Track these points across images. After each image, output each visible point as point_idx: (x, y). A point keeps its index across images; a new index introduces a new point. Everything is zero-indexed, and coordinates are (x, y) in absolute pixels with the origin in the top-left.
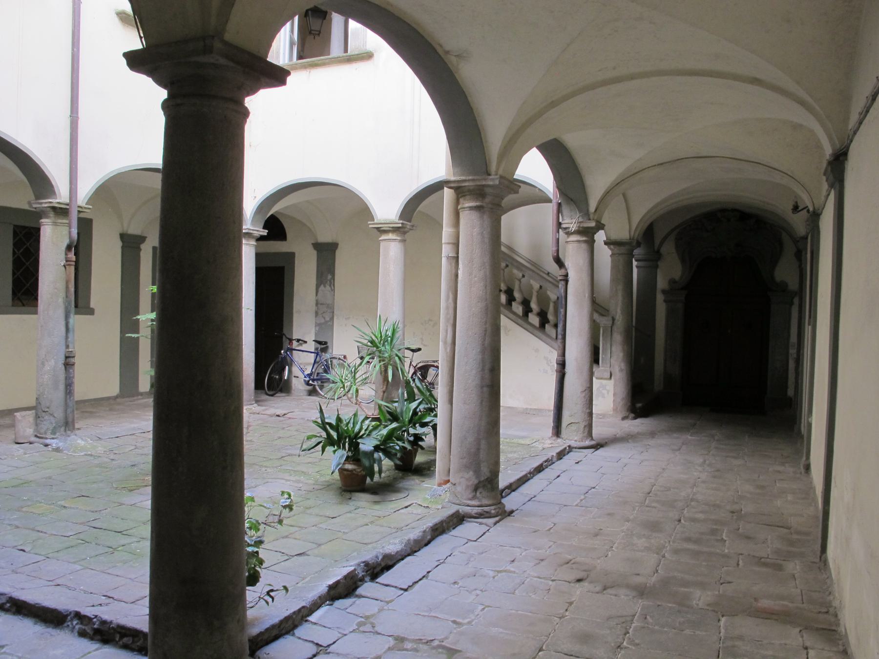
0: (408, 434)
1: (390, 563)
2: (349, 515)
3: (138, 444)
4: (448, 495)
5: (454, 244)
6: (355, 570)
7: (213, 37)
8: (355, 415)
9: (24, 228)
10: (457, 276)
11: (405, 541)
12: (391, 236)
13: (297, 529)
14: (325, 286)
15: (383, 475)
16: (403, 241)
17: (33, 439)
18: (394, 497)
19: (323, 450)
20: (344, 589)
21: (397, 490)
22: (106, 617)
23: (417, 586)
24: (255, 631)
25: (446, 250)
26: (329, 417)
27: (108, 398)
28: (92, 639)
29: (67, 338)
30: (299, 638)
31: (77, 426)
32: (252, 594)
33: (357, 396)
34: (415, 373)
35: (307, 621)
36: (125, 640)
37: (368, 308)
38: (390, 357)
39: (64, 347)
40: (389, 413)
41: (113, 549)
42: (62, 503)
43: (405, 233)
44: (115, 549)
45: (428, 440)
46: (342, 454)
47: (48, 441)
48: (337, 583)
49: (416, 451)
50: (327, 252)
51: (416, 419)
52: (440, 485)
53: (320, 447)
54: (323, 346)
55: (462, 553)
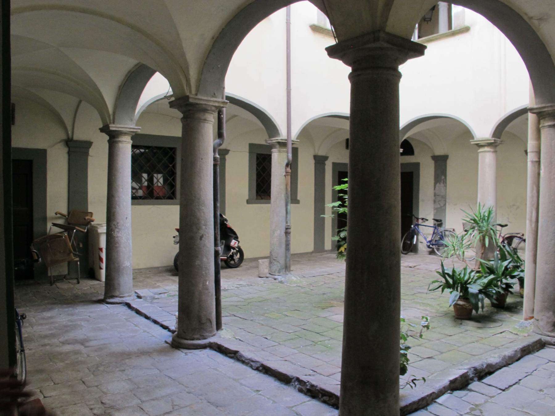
0: (501, 282)
1: (492, 370)
2: (461, 335)
3: (326, 281)
4: (533, 327)
5: (536, 152)
6: (467, 372)
7: (379, 31)
8: (465, 269)
9: (262, 155)
10: (539, 174)
11: (502, 357)
12: (486, 149)
13: (426, 341)
14: (440, 184)
15: (484, 310)
16: (495, 152)
17: (268, 275)
18: (492, 325)
19: (443, 291)
20: (460, 384)
21: (494, 321)
22: (314, 383)
23: (512, 388)
24: (403, 404)
25: (531, 157)
26: (447, 270)
27: (307, 253)
28: (306, 394)
29: (286, 217)
30: (431, 413)
31: (292, 269)
32: (403, 380)
33: (463, 256)
34: (503, 241)
35: (435, 402)
36: (325, 398)
37: (471, 197)
38: (487, 230)
39: (285, 223)
40: (488, 268)
41: (315, 343)
42: (285, 313)
43: (496, 146)
44: (316, 343)
45: (516, 288)
46: (457, 294)
47: (276, 277)
48: (456, 379)
49: (507, 295)
50: (441, 162)
51: (507, 273)
52: (526, 319)
53: (440, 289)
54: (439, 223)
55: (545, 369)
